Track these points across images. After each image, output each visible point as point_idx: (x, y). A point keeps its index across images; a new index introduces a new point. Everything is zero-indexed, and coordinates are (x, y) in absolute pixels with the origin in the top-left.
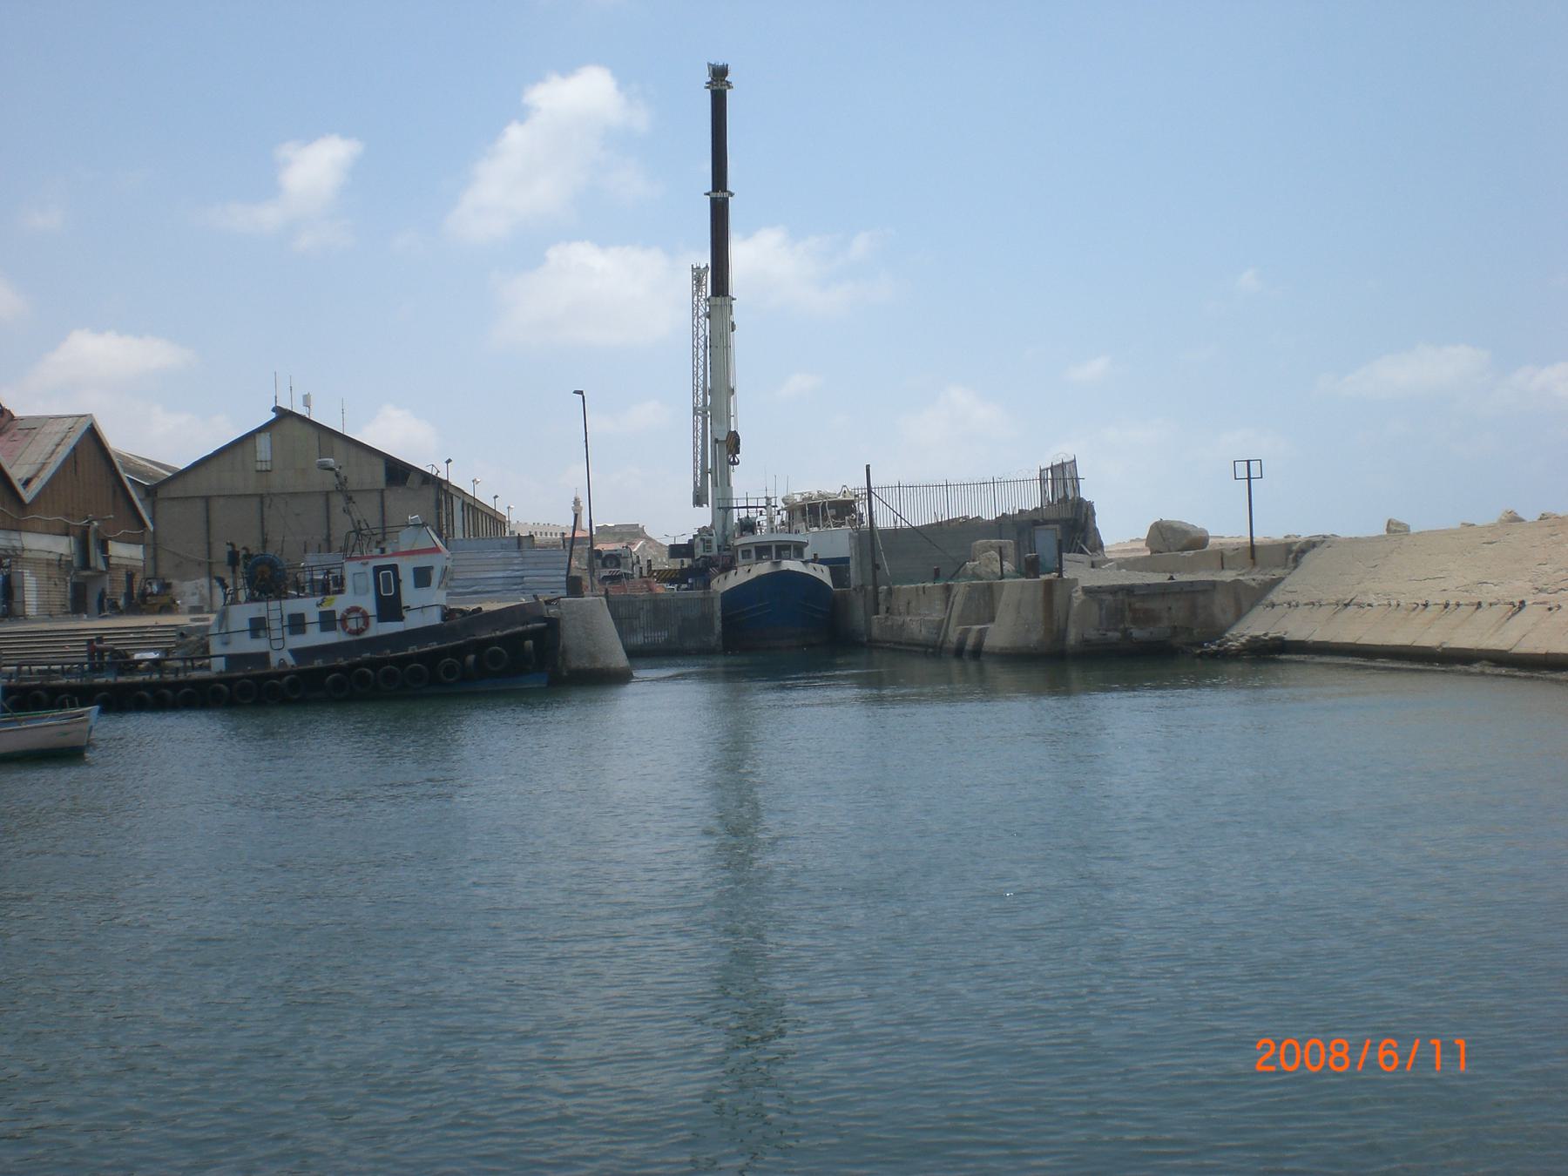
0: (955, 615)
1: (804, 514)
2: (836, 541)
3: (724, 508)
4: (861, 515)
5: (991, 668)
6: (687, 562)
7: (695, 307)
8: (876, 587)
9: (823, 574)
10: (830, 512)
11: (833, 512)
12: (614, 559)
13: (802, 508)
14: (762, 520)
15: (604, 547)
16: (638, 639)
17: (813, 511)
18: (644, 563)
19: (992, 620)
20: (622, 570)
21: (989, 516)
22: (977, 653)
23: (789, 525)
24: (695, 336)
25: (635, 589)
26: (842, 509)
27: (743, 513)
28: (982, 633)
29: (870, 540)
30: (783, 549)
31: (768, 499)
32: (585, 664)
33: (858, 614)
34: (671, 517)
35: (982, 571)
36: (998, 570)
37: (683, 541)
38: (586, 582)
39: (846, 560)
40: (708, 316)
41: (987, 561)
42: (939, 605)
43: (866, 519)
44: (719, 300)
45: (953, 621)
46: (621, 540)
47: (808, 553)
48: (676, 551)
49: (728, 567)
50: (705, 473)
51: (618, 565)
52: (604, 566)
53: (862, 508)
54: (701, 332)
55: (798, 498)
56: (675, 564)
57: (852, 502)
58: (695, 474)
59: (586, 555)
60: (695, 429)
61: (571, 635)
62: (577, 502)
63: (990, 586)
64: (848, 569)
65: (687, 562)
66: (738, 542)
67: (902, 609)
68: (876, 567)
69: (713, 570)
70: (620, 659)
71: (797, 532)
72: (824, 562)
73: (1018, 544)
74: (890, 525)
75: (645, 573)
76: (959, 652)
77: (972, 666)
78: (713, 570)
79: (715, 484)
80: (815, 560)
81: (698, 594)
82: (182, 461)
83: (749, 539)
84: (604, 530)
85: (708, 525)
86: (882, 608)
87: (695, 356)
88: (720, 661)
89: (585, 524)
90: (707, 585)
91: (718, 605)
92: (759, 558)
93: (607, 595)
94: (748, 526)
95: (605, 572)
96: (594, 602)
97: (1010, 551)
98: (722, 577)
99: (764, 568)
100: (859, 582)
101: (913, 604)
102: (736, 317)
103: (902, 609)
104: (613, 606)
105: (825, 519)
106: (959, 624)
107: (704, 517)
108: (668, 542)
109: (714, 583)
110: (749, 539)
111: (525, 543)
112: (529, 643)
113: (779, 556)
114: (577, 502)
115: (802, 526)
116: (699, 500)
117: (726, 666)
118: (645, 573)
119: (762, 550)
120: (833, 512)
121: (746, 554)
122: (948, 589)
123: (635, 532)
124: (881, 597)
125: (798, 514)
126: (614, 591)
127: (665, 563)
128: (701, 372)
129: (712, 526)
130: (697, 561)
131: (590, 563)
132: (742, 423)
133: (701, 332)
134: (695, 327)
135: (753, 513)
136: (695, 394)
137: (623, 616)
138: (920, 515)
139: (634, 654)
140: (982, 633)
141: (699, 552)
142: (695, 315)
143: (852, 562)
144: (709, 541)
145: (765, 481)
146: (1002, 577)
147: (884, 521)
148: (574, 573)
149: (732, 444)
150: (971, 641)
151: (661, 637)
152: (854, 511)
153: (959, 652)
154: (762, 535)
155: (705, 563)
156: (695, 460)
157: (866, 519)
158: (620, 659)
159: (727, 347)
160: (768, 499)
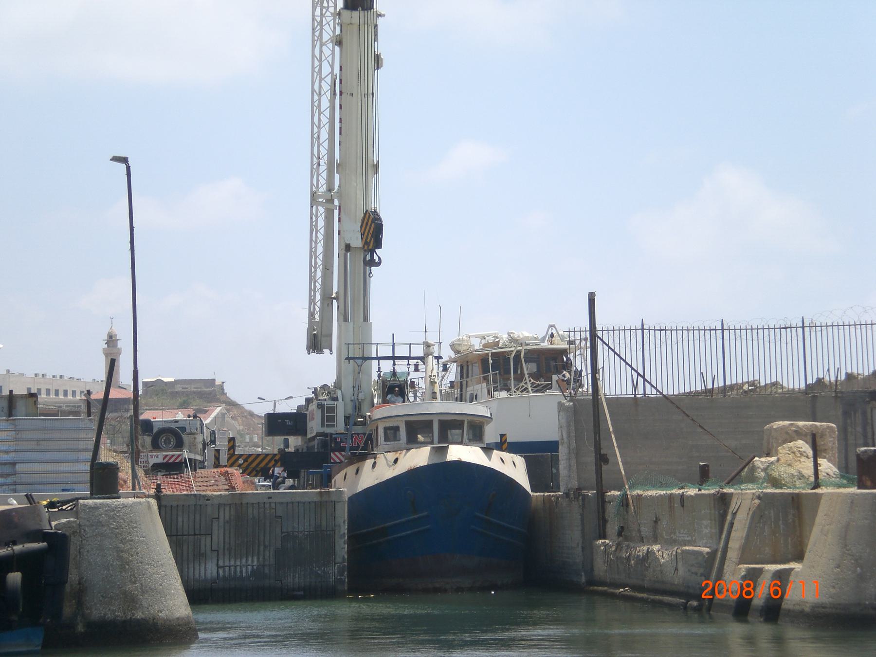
0: (735, 545)
1: (485, 370)
2: (537, 413)
3: (357, 358)
4: (579, 374)
5: (794, 634)
6: (295, 442)
7: (317, 26)
8: (601, 494)
9: (514, 468)
10: (528, 368)
11: (533, 367)
12: (174, 435)
13: (484, 360)
14: (418, 378)
15: (158, 416)
16: (209, 570)
17: (499, 366)
18: (222, 444)
19: (799, 557)
20: (186, 454)
21: (794, 381)
22: (773, 611)
23: (460, 390)
24: (316, 73)
25: (206, 484)
26: (546, 364)
27: (387, 367)
28: (782, 577)
29: (589, 414)
30: (451, 428)
31: (427, 345)
32: (114, 611)
33: (572, 536)
34: (274, 371)
35: (781, 471)
36: (809, 471)
37: (288, 407)
38: (125, 473)
39: (552, 446)
40: (339, 42)
41: (794, 462)
42: (707, 528)
43: (587, 381)
44: (356, 16)
45: (733, 554)
46: (183, 406)
47: (491, 435)
48: (277, 423)
49: (362, 451)
50: (327, 299)
51: (179, 445)
52: (156, 446)
53: (580, 362)
54: (326, 69)
55: (477, 344)
56: (273, 445)
57: (564, 352)
58: (312, 301)
59: (127, 427)
60: (313, 228)
61: (87, 565)
62: (111, 340)
63: (796, 500)
64: (555, 461)
65: (295, 442)
66: (378, 414)
67: (646, 531)
68: (602, 459)
69: (335, 456)
70: (175, 604)
71: (473, 398)
72: (515, 448)
73: (844, 431)
74: (626, 391)
75: (224, 458)
76: (742, 609)
77: (763, 630)
78: (335, 456)
79: (344, 317)
80: (503, 445)
81: (312, 492)
82: (335, 378)
83: (397, 409)
84: (158, 389)
85: (330, 381)
86: (612, 528)
87: (315, 107)
88: (346, 610)
89: (124, 376)
90: (327, 480)
91: (343, 514)
92: (412, 442)
93: (158, 496)
94: (395, 388)
95: (158, 457)
96: (138, 506)
97: (831, 442)
98: (351, 470)
99: (419, 457)
100: (575, 484)
101: (664, 523)
102: (382, 47)
103: (646, 531)
104: (169, 510)
105: (520, 378)
106: (742, 561)
107: (324, 369)
108: (263, 410)
109: (338, 478)
110: (397, 409)
111: (20, 406)
112: (15, 577)
113: (445, 438)
114: (111, 340)
115: (481, 389)
116: (316, 343)
117: (357, 619)
118: (224, 458)
119: (416, 430)
120: (533, 367)
121: (392, 433)
122: (723, 500)
123: (208, 392)
124: (611, 510)
125: (476, 369)
126: (172, 488)
127: (257, 443)
128: (324, 135)
129: (338, 385)
130: (310, 442)
131: (133, 440)
132: (390, 200)
133: (326, 69)
134: (317, 60)
135: (402, 367)
136: (314, 169)
137: (185, 525)
138: (677, 375)
139: (198, 595)
140: (782, 577)
141: (314, 426)
142: (317, 39)
143: (563, 451)
144: (332, 409)
145: (432, 306)
146: (817, 485)
147: (616, 384)
148: (105, 457)
149: (373, 230)
150: (761, 594)
151: (246, 566)
152: (567, 366)
153: (742, 609)
154: (416, 405)
155: (324, 445)
156: (312, 278)
157: (587, 381)
158: (175, 604)
159: (368, 95)
160: (427, 345)
